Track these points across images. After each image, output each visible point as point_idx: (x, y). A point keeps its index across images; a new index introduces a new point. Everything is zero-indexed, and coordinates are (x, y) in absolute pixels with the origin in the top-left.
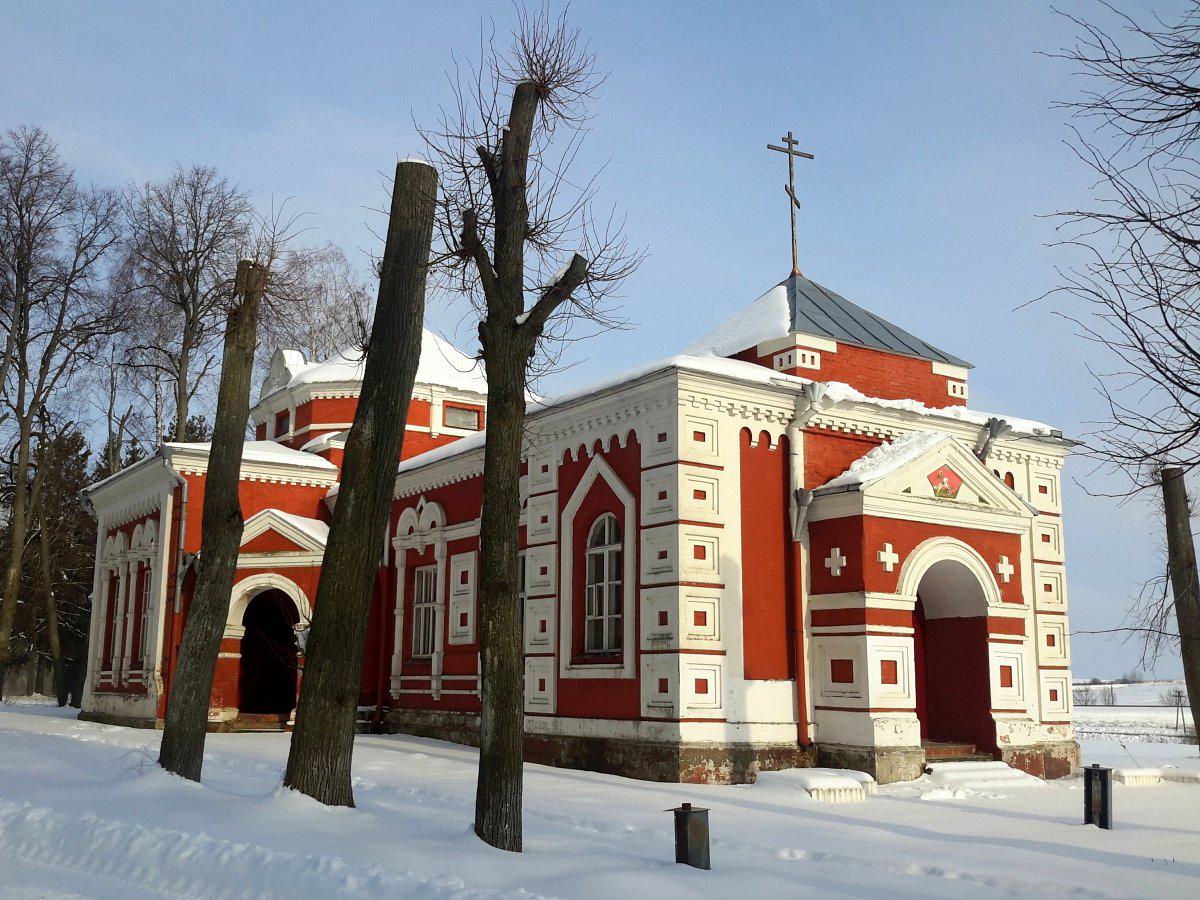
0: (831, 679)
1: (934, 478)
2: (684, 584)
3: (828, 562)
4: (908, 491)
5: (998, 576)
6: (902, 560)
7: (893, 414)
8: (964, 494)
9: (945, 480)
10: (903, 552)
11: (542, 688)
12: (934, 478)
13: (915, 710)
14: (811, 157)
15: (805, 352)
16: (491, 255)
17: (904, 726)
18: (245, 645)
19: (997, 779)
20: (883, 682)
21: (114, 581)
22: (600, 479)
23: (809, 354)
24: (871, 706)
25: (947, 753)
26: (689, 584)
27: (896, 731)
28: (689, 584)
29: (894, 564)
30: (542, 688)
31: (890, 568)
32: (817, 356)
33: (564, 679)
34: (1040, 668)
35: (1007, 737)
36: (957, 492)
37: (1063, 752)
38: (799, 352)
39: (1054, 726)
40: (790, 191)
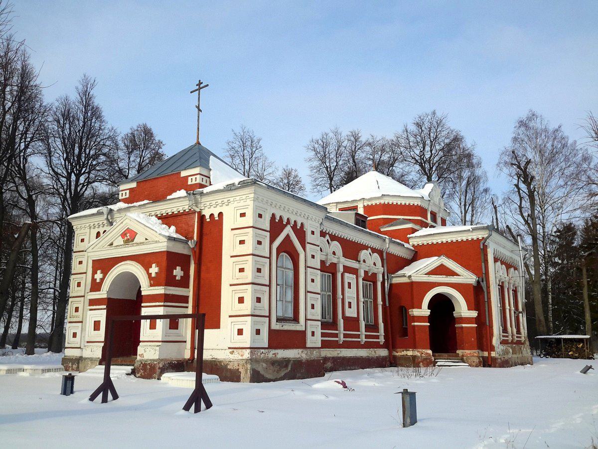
0: (219, 330)
3: (182, 273)
4: (112, 244)
5: (149, 275)
7: (147, 206)
8: (120, 241)
9: (128, 235)
10: (105, 273)
12: (123, 235)
13: (140, 342)
14: (191, 92)
16: (73, 194)
17: (95, 349)
18: (430, 319)
19: (99, 373)
20: (219, 327)
21: (502, 288)
22: (288, 236)
25: (130, 362)
26: (74, 297)
27: (91, 351)
28: (74, 297)
31: (98, 281)
33: (274, 330)
34: (82, 322)
35: (142, 354)
37: (236, 365)
39: (235, 350)
40: (198, 107)
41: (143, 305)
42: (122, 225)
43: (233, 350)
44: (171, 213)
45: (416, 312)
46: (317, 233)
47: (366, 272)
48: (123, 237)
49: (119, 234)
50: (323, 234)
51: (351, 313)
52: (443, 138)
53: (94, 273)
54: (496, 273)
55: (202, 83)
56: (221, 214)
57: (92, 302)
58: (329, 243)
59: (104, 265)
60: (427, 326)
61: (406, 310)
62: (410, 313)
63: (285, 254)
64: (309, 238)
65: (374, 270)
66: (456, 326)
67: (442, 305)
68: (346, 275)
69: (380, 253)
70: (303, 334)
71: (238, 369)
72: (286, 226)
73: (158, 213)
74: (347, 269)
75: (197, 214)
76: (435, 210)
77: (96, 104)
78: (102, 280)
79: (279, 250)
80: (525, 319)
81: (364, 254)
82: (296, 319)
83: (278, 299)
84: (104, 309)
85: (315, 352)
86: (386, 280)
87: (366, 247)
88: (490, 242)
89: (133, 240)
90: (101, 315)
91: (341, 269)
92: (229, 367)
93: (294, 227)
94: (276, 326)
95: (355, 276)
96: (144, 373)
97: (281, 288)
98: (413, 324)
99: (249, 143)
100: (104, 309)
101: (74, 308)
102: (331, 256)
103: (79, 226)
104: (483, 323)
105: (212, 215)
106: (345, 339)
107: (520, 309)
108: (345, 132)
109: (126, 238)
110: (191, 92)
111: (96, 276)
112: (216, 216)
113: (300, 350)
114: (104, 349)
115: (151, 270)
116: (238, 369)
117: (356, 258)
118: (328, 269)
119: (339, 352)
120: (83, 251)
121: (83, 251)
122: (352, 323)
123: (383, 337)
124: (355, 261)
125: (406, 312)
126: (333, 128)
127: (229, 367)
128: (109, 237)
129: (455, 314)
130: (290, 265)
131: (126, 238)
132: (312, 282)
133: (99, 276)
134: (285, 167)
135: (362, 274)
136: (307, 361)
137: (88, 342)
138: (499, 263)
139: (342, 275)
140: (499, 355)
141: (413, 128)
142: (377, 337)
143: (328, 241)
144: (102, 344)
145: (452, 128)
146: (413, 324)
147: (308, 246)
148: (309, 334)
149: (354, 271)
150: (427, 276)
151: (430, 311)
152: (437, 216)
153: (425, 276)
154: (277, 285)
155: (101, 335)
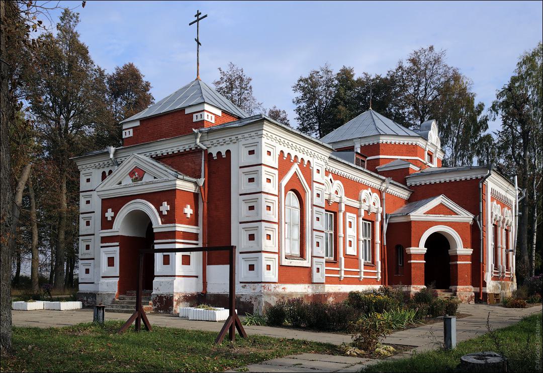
1: (131, 174)
2: (264, 221)
4: (120, 183)
5: (160, 213)
6: (115, 215)
9: (136, 174)
10: (116, 212)
11: (318, 269)
12: (131, 174)
14: (190, 24)
15: (209, 114)
18: (427, 256)
21: (496, 227)
22: (424, 159)
23: (210, 115)
24: (176, 275)
29: (112, 217)
30: (318, 269)
32: (213, 117)
36: (142, 178)
38: (206, 113)
39: (247, 284)
40: (199, 43)
41: (155, 241)
42: (129, 164)
43: (245, 284)
44: (177, 152)
45: (413, 250)
46: (323, 172)
47: (367, 212)
48: (131, 177)
49: (127, 174)
50: (327, 173)
51: (351, 251)
52: (439, 76)
53: (104, 211)
54: (492, 210)
55: (200, 14)
56: (228, 152)
57: (104, 239)
58: (332, 182)
59: (114, 203)
60: (468, 264)
61: (403, 248)
62: (407, 252)
63: (292, 192)
64: (316, 177)
65: (373, 210)
66: (451, 263)
67: (439, 243)
68: (348, 214)
69: (380, 192)
70: (310, 269)
71: (251, 302)
72: (292, 164)
73: (153, 153)
74: (349, 208)
75: (203, 153)
76: (433, 150)
77: (81, 42)
78: (113, 218)
79: (287, 189)
80: (514, 257)
81: (364, 194)
82: (302, 256)
83: (286, 237)
84: (117, 246)
85: (320, 287)
86: (385, 220)
87: (366, 187)
88: (488, 181)
89: (141, 179)
90: (115, 251)
91: (343, 208)
92: (241, 300)
93: (301, 165)
94: (285, 262)
95: (355, 216)
96: (160, 305)
97: (289, 227)
98: (409, 262)
99: (237, 83)
100: (117, 246)
101: (271, 238)
102: (334, 196)
103: (84, 166)
104: (477, 260)
105: (219, 153)
106: (345, 276)
107: (511, 248)
108: (336, 70)
109: (134, 177)
110: (190, 24)
111: (107, 215)
112: (224, 153)
113: (307, 285)
114: (120, 283)
115: (161, 209)
116: (251, 302)
117: (357, 197)
118: (333, 210)
119: (340, 288)
120: (92, 191)
121: (92, 191)
122: (352, 260)
123: (379, 274)
124: (356, 201)
125: (403, 250)
126: (323, 66)
127: (241, 300)
128: (117, 176)
129: (451, 252)
130: (296, 203)
131: (134, 177)
132: (319, 222)
133: (109, 214)
134: (272, 109)
135: (363, 214)
136: (313, 295)
137: (103, 277)
138: (495, 203)
139: (344, 215)
140: (490, 291)
141: (407, 65)
142: (375, 274)
143: (331, 180)
144: (117, 280)
145: (450, 66)
146: (409, 262)
147: (315, 185)
148: (315, 270)
149: (356, 211)
150: (425, 215)
151: (472, 250)
152: (434, 155)
153: (424, 215)
154: (286, 223)
155: (116, 270)
